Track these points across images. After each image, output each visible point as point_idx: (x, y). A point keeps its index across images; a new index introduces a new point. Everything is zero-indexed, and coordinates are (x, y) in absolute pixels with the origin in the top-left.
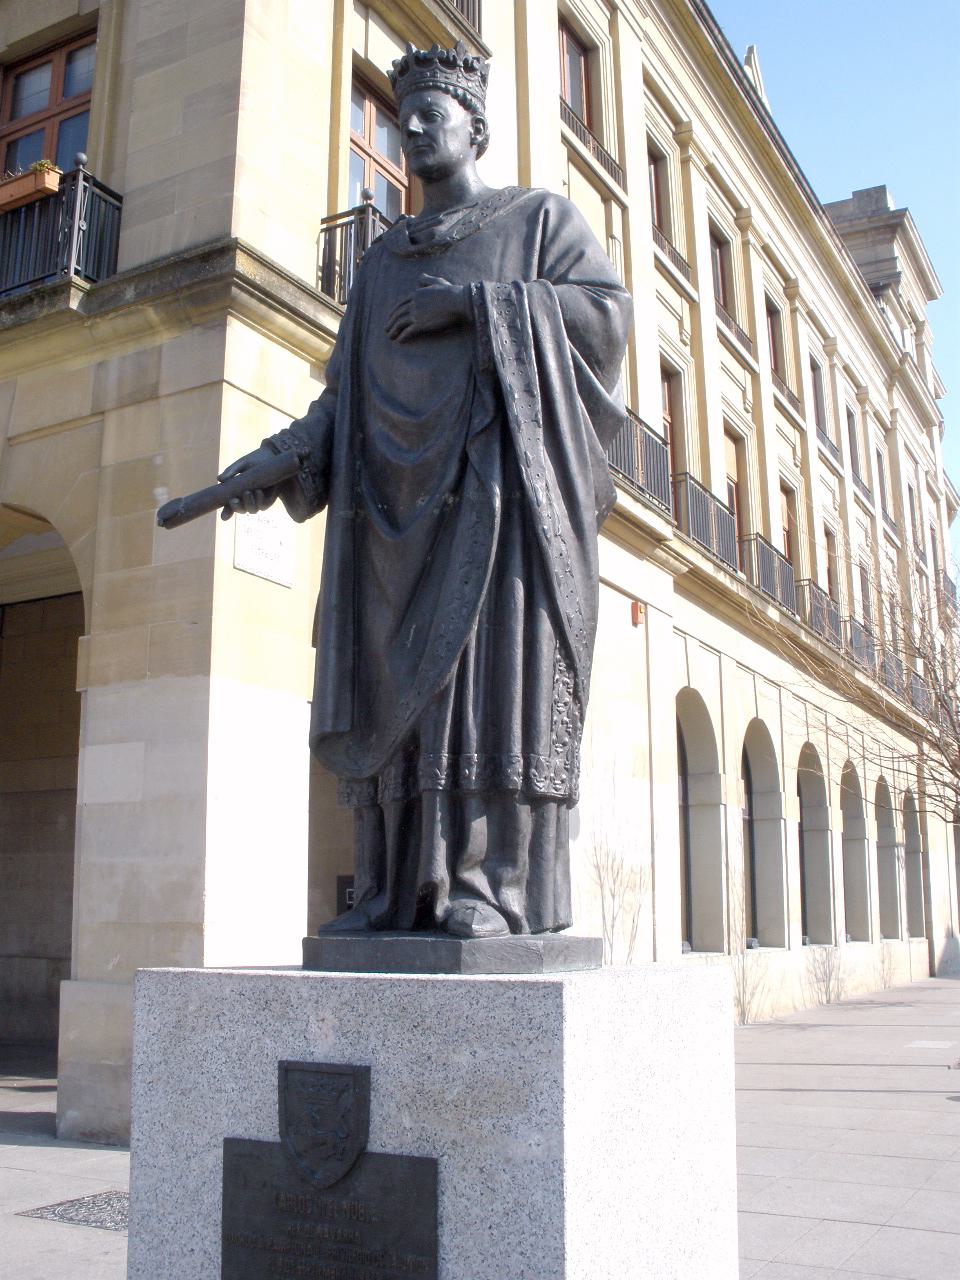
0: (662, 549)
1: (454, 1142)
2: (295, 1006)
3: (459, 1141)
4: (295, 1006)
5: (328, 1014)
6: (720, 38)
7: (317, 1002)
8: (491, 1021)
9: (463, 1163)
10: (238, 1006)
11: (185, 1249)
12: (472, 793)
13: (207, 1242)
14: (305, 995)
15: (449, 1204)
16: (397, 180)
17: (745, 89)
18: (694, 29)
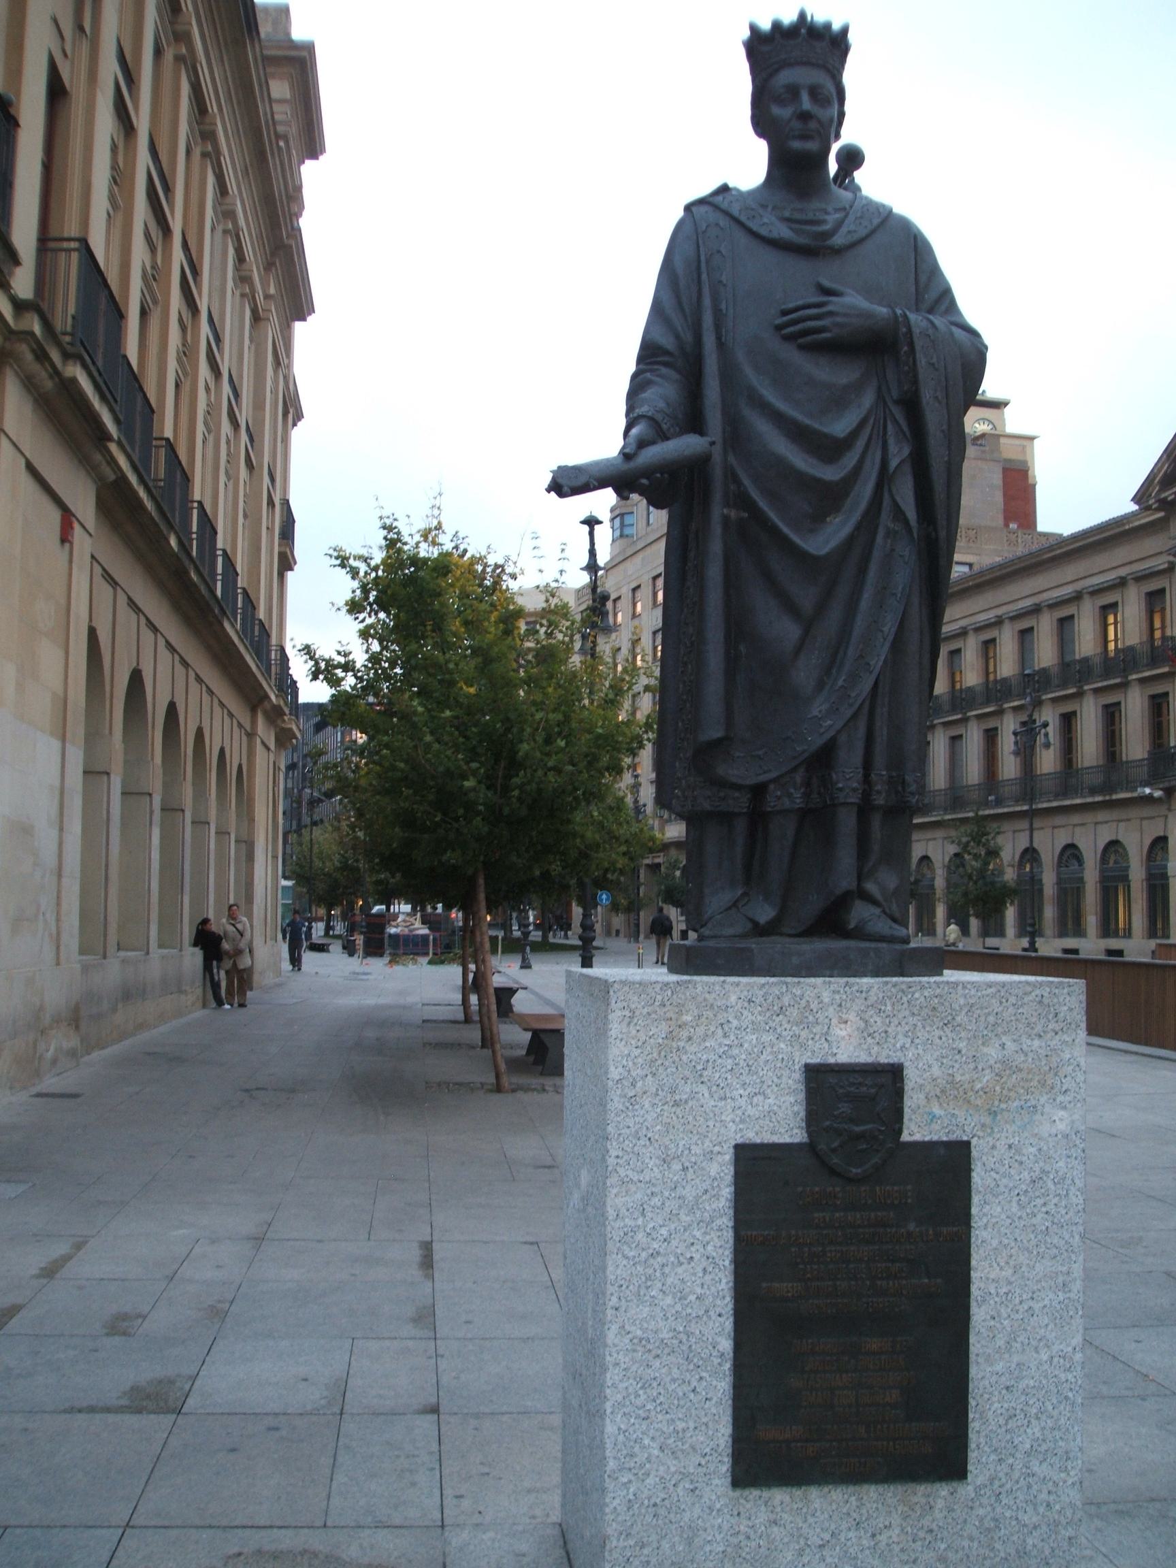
2: (815, 1010)
4: (815, 1010)
7: (840, 1005)
10: (745, 1013)
14: (826, 1000)
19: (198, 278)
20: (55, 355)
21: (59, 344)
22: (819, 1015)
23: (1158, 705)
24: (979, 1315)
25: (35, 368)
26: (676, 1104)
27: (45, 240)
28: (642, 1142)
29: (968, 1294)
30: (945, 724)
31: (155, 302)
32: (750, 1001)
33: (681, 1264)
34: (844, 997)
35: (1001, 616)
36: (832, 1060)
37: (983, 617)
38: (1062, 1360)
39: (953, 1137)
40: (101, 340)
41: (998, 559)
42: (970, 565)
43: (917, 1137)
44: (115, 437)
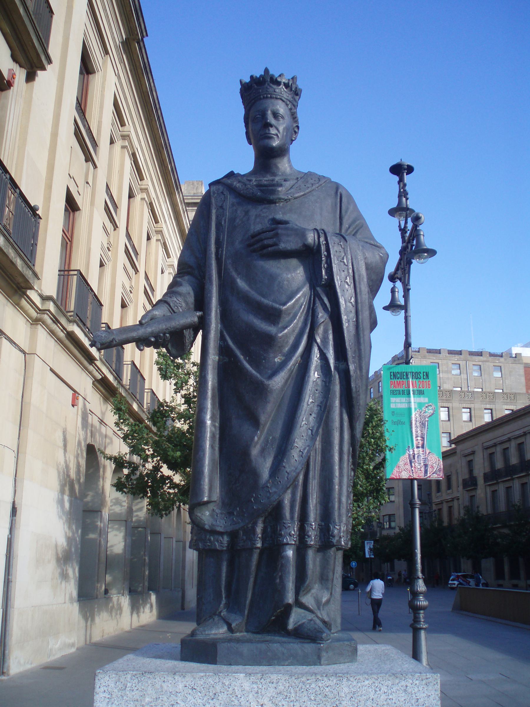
0: (93, 366)
2: (239, 696)
4: (239, 696)
6: (152, 84)
7: (257, 693)
8: (390, 702)
10: (189, 697)
12: (310, 546)
14: (247, 688)
17: (158, 115)
18: (141, 76)
19: (154, 293)
20: (63, 321)
22: (242, 699)
23: (524, 485)
25: (54, 327)
30: (503, 481)
31: (131, 302)
34: (260, 686)
37: (517, 433)
42: (512, 410)
44: (98, 358)
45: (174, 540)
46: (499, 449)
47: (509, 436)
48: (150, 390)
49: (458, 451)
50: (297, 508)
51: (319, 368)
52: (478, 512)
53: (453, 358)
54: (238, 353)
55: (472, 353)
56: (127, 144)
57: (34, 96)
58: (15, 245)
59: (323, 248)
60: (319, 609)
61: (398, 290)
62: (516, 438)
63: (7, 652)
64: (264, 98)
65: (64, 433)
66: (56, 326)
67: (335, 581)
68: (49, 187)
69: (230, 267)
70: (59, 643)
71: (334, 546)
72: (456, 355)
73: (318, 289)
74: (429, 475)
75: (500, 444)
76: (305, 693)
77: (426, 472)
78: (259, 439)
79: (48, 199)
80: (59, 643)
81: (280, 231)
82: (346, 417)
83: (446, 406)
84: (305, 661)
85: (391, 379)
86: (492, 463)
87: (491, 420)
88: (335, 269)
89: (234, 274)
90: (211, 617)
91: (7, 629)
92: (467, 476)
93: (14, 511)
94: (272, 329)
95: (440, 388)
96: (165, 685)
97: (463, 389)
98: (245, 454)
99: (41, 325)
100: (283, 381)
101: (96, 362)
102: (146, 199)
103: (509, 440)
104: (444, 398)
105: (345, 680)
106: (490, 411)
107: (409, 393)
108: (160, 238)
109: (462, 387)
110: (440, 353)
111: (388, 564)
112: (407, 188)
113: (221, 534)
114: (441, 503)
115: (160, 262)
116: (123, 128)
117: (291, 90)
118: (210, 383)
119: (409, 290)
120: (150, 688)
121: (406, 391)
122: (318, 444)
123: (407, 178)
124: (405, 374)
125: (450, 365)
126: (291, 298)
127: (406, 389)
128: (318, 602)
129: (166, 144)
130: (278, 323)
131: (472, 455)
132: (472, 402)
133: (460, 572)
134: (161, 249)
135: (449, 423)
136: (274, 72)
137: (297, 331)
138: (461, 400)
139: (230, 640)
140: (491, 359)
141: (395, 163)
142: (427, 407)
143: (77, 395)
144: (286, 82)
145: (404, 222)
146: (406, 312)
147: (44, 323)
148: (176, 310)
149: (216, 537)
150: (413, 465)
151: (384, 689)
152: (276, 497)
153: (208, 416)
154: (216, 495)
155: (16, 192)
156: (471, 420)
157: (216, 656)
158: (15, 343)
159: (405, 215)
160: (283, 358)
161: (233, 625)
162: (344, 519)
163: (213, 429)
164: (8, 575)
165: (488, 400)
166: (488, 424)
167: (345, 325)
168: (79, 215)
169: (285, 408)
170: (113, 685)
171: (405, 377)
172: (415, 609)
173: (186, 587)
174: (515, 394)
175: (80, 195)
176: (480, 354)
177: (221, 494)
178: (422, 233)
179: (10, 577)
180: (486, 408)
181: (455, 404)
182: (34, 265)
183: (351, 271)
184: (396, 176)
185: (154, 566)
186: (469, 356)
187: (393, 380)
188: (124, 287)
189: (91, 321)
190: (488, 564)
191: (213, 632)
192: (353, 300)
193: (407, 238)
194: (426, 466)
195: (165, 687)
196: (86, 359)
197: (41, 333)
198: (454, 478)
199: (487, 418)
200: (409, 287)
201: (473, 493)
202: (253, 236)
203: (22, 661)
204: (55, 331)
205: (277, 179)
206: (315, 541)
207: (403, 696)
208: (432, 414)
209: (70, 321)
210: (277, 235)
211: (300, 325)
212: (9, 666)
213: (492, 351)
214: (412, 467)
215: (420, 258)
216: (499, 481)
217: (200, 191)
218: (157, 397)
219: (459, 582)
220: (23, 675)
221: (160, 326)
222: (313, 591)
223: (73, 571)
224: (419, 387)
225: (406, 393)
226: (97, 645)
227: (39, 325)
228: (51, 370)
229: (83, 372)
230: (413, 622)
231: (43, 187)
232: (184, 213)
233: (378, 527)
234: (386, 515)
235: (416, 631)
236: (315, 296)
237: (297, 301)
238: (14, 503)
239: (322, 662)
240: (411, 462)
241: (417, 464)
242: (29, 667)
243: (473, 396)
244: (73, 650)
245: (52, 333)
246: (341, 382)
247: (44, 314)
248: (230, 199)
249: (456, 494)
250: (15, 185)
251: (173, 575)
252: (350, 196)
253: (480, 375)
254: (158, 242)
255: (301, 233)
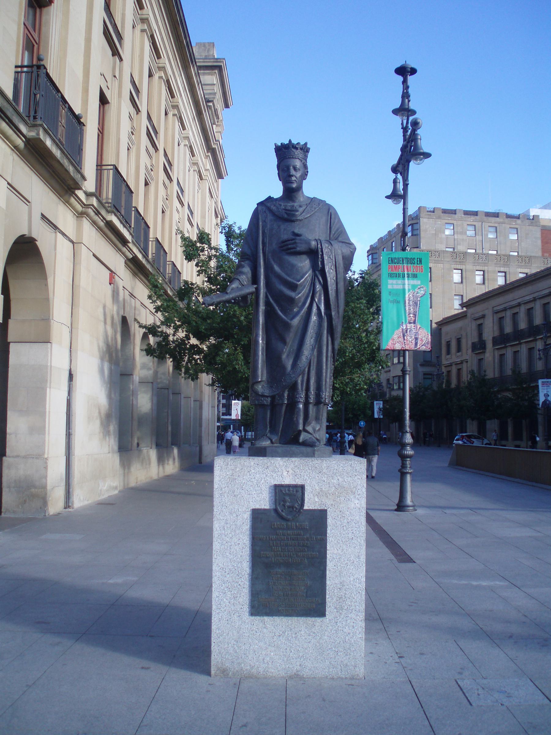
0: (126, 248)
1: (332, 504)
3: (334, 504)
5: (290, 470)
9: (335, 510)
11: (236, 544)
12: (311, 403)
13: (245, 541)
15: (330, 521)
16: (34, 39)
20: (103, 212)
21: (104, 207)
24: (330, 565)
25: (96, 218)
26: (235, 496)
27: (100, 167)
28: (224, 507)
29: (326, 557)
31: (152, 179)
32: (258, 464)
33: (236, 545)
35: (535, 298)
36: (283, 483)
37: (528, 298)
38: (357, 580)
39: (321, 508)
40: (123, 204)
41: (538, 270)
42: (527, 274)
43: (312, 507)
44: (131, 241)
45: (192, 400)
46: (509, 313)
47: (519, 301)
48: (171, 263)
49: (469, 315)
50: (305, 385)
51: (316, 314)
52: (485, 375)
53: (469, 219)
54: (275, 305)
55: (488, 214)
56: (146, 27)
57: (71, 7)
58: (69, 156)
59: (320, 250)
60: (315, 432)
61: (421, 137)
62: (526, 303)
63: (71, 490)
64: (288, 158)
65: (104, 307)
66: (97, 217)
67: (323, 420)
68: (86, 91)
69: (270, 257)
70: (106, 485)
71: (322, 403)
72: (472, 216)
73: (317, 272)
74: (418, 347)
75: (510, 308)
76: (307, 466)
77: (416, 344)
78: (286, 350)
79: (85, 102)
80: (106, 485)
81: (297, 241)
82: (330, 339)
83: (460, 268)
84: (307, 455)
85: (389, 263)
86: (501, 328)
87: (504, 284)
88: (325, 262)
89: (272, 262)
90: (262, 437)
91: (70, 472)
92: (476, 340)
93: (71, 377)
94: (292, 294)
95: (454, 250)
96: (245, 463)
97: (477, 251)
98: (279, 358)
99: (85, 217)
100: (298, 321)
101: (128, 244)
102: (164, 77)
103: (519, 305)
104: (458, 260)
105: (324, 461)
106: (503, 274)
107: (404, 277)
108: (176, 113)
109: (477, 249)
110: (455, 214)
111: (397, 424)
112: (410, 90)
113: (267, 397)
114: (451, 365)
115: (177, 136)
116: (142, 11)
117: (304, 151)
118: (261, 321)
119: (407, 185)
120: (239, 465)
121: (401, 275)
122: (315, 353)
123: (410, 78)
124: (401, 259)
125: (465, 226)
126: (302, 278)
127: (402, 273)
128: (314, 430)
129: (187, 43)
130: (296, 291)
131: (483, 319)
132: (485, 264)
133: (466, 432)
134: (177, 124)
135: (461, 285)
136: (294, 142)
137: (305, 295)
138: (474, 263)
139: (272, 447)
140: (507, 220)
141: (399, 66)
142: (419, 289)
143: (114, 274)
144: (301, 147)
145: (406, 120)
146: (404, 204)
147: (88, 215)
148: (243, 284)
149: (265, 398)
150: (405, 338)
151: (342, 465)
152: (294, 379)
153: (260, 339)
154: (265, 378)
155: (66, 107)
156: (484, 283)
157: (266, 453)
158: (66, 235)
159: (406, 115)
160: (298, 309)
161: (273, 440)
162: (328, 390)
163: (263, 345)
164: (69, 429)
165: (502, 262)
166: (501, 287)
167: (330, 292)
168: (109, 107)
169: (299, 334)
170: (222, 463)
171: (401, 262)
172: (403, 457)
173: (203, 444)
174: (530, 258)
175: (109, 89)
176: (496, 215)
177: (267, 378)
178: (419, 137)
179: (70, 431)
180: (500, 271)
181: (469, 266)
182: (81, 168)
183: (334, 262)
184: (401, 76)
185: (176, 424)
186: (484, 217)
187: (391, 265)
188: (146, 167)
189: (125, 209)
190: (492, 425)
191: (264, 443)
192: (335, 278)
193: (407, 137)
194: (416, 339)
195: (246, 464)
196: (120, 242)
197: (86, 224)
198: (464, 341)
199: (501, 281)
200: (408, 183)
201: (481, 357)
202: (283, 242)
203: (82, 498)
204: (97, 222)
205: (296, 204)
206: (313, 400)
207: (350, 468)
208: (424, 295)
209: (108, 212)
210: (295, 243)
211: (307, 291)
212: (73, 502)
213: (510, 213)
214: (404, 339)
215: (416, 160)
216: (507, 345)
217: (211, 53)
218: (177, 268)
219: (464, 442)
220: (84, 508)
221: (237, 294)
222: (312, 424)
223: (113, 427)
224: (413, 272)
225: (401, 276)
226: (132, 489)
227: (84, 218)
228: (94, 255)
229: (117, 253)
230: (401, 468)
231: (81, 91)
232: (199, 84)
233: (388, 388)
234: (396, 376)
235: (403, 475)
236: (315, 276)
237: (306, 279)
238: (70, 371)
239: (315, 456)
240: (404, 336)
241: (408, 337)
242: (86, 503)
243: (487, 258)
244: (116, 492)
245: (94, 223)
246: (327, 321)
247: (89, 208)
248: (270, 217)
249: (465, 357)
250: (65, 101)
251: (191, 431)
252: (336, 213)
253: (495, 237)
254: (174, 117)
255: (308, 242)
